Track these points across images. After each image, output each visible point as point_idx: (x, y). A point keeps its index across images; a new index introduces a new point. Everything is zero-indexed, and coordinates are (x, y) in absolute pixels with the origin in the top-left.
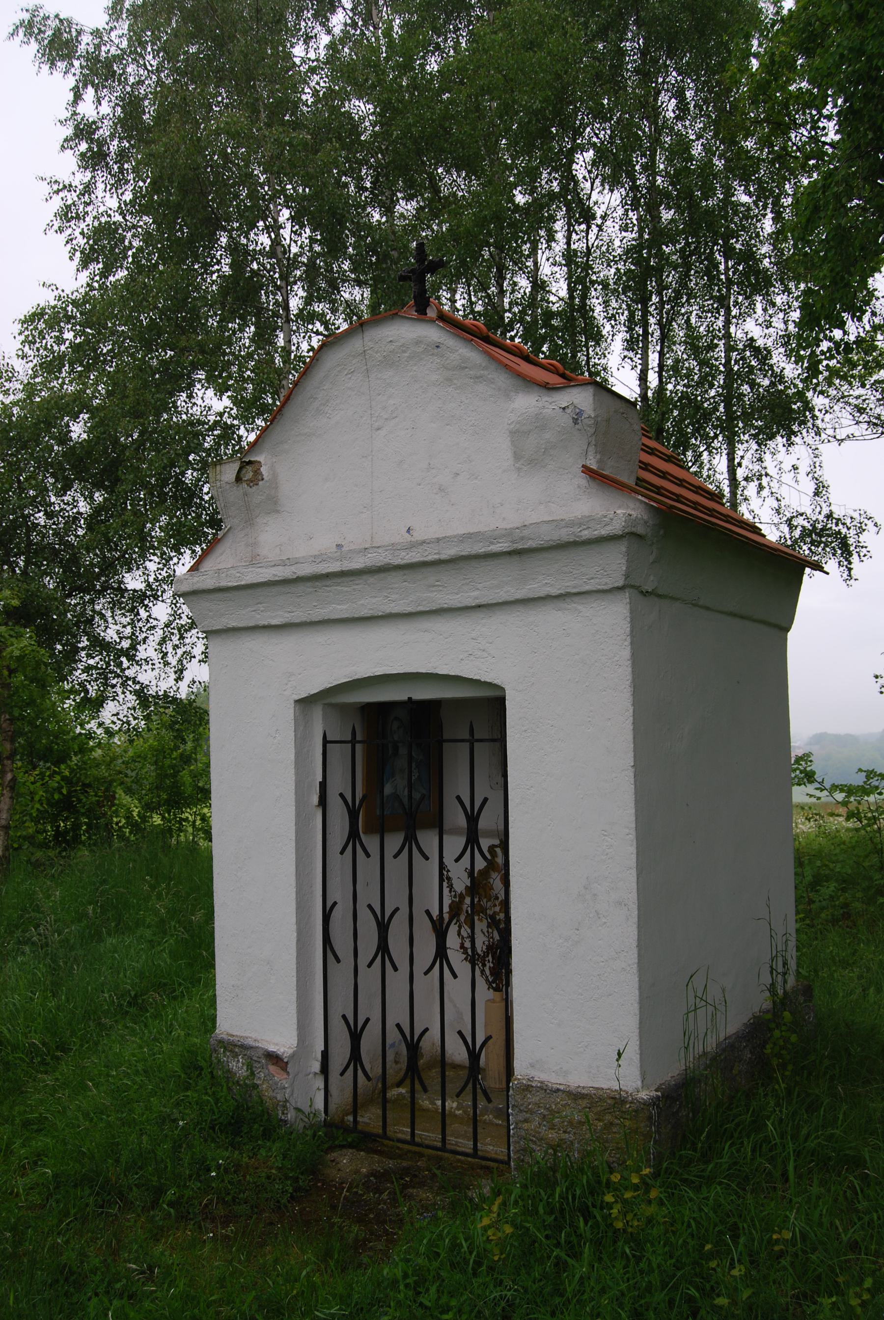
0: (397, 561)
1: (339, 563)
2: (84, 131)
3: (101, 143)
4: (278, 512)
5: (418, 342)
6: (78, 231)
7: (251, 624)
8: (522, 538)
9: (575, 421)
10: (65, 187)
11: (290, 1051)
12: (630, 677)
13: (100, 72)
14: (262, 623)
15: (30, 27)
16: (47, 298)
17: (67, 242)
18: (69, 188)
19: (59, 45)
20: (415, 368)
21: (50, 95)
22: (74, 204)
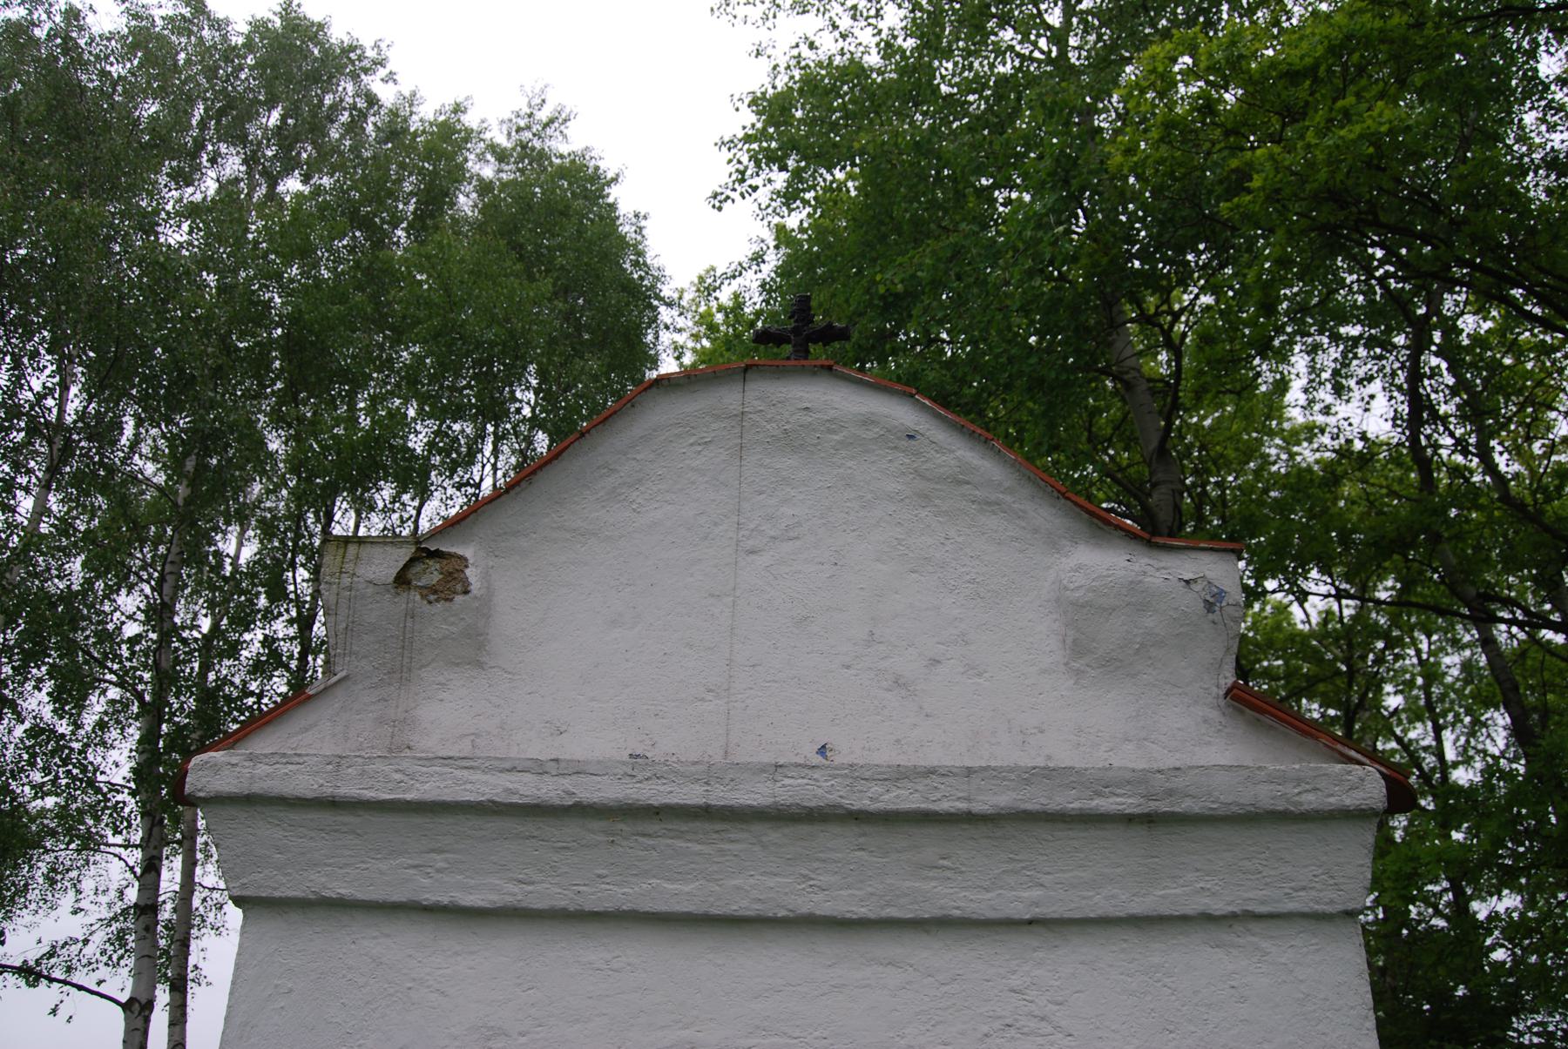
4: (480, 665)
5: (868, 421)
7: (397, 897)
8: (1170, 793)
9: (1209, 606)
14: (430, 897)
20: (850, 464)
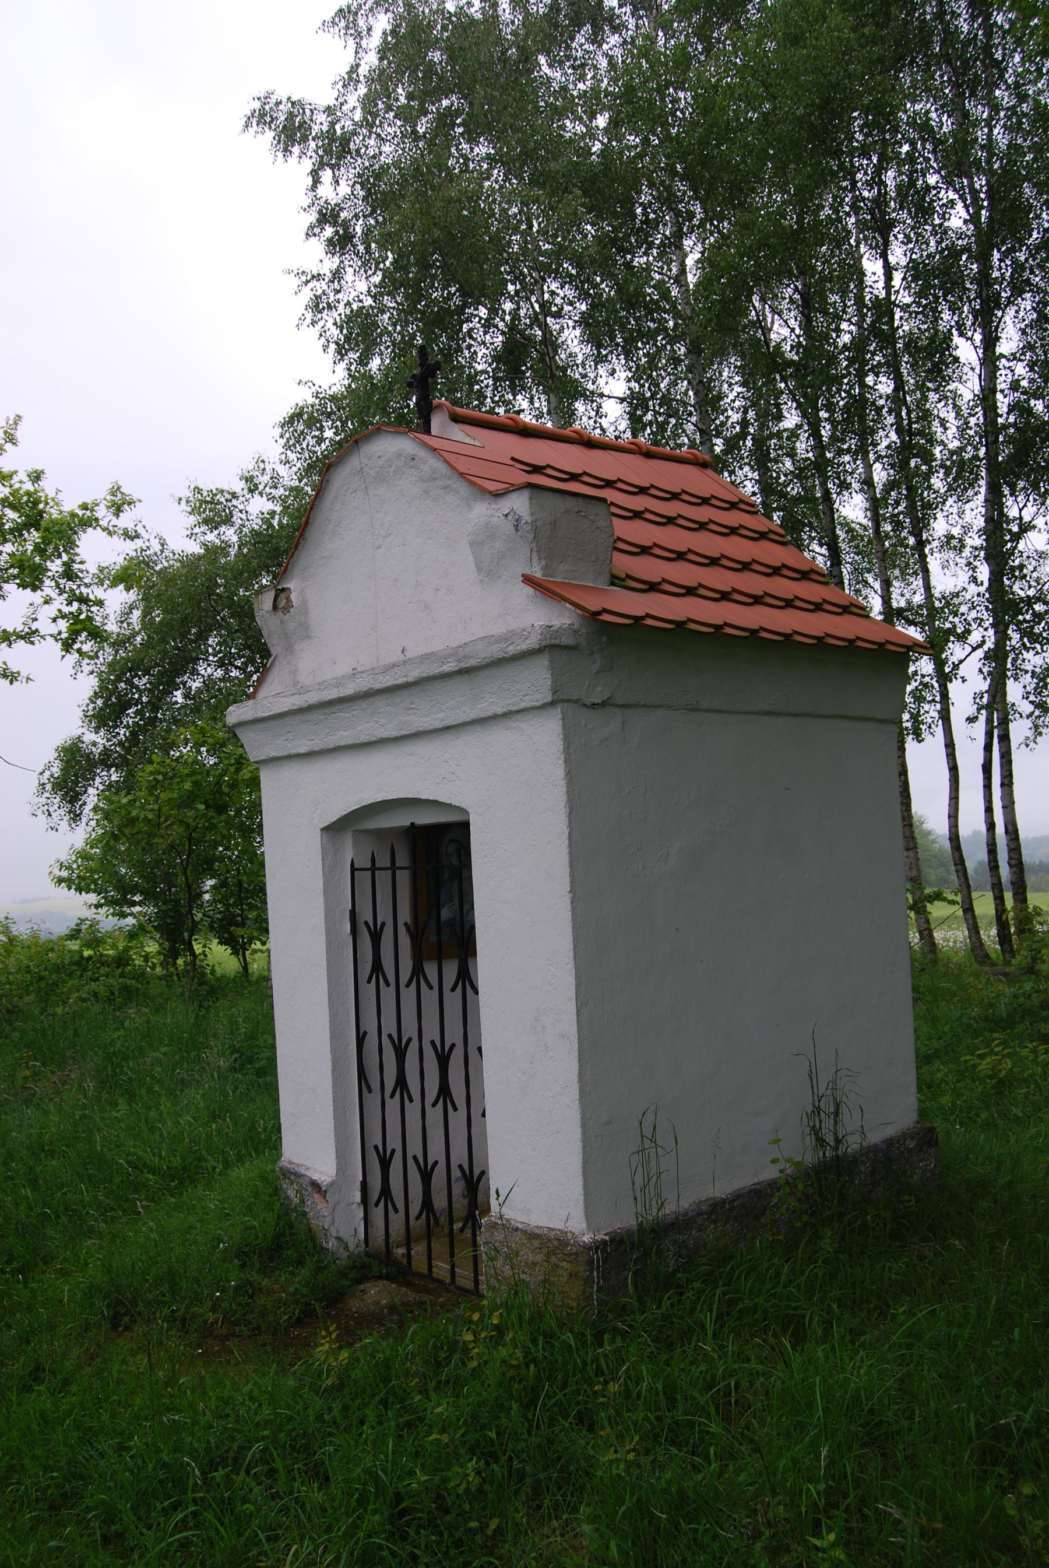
0: (377, 686)
1: (336, 690)
2: (327, 216)
3: (346, 224)
4: (309, 637)
6: (331, 321)
8: (465, 657)
9: (516, 528)
10: (313, 277)
11: (329, 1180)
12: (565, 798)
13: (336, 150)
14: (294, 752)
15: (262, 117)
16: (305, 397)
17: (321, 335)
18: (318, 277)
19: (290, 128)
21: (286, 188)
22: (324, 293)
